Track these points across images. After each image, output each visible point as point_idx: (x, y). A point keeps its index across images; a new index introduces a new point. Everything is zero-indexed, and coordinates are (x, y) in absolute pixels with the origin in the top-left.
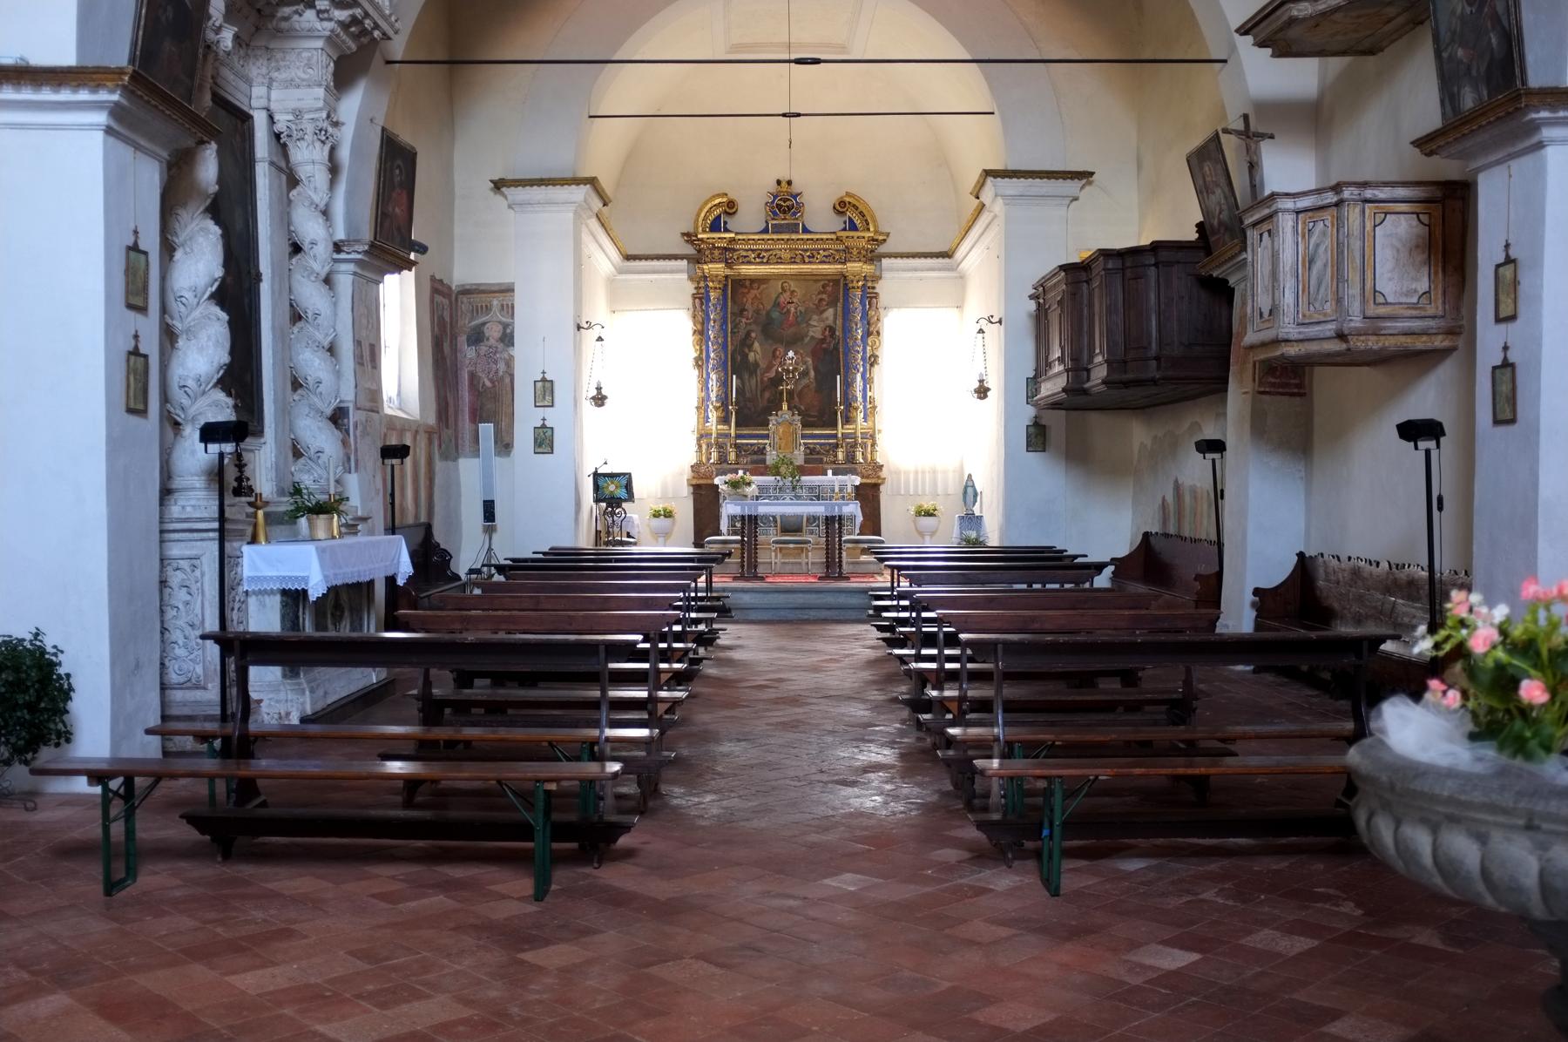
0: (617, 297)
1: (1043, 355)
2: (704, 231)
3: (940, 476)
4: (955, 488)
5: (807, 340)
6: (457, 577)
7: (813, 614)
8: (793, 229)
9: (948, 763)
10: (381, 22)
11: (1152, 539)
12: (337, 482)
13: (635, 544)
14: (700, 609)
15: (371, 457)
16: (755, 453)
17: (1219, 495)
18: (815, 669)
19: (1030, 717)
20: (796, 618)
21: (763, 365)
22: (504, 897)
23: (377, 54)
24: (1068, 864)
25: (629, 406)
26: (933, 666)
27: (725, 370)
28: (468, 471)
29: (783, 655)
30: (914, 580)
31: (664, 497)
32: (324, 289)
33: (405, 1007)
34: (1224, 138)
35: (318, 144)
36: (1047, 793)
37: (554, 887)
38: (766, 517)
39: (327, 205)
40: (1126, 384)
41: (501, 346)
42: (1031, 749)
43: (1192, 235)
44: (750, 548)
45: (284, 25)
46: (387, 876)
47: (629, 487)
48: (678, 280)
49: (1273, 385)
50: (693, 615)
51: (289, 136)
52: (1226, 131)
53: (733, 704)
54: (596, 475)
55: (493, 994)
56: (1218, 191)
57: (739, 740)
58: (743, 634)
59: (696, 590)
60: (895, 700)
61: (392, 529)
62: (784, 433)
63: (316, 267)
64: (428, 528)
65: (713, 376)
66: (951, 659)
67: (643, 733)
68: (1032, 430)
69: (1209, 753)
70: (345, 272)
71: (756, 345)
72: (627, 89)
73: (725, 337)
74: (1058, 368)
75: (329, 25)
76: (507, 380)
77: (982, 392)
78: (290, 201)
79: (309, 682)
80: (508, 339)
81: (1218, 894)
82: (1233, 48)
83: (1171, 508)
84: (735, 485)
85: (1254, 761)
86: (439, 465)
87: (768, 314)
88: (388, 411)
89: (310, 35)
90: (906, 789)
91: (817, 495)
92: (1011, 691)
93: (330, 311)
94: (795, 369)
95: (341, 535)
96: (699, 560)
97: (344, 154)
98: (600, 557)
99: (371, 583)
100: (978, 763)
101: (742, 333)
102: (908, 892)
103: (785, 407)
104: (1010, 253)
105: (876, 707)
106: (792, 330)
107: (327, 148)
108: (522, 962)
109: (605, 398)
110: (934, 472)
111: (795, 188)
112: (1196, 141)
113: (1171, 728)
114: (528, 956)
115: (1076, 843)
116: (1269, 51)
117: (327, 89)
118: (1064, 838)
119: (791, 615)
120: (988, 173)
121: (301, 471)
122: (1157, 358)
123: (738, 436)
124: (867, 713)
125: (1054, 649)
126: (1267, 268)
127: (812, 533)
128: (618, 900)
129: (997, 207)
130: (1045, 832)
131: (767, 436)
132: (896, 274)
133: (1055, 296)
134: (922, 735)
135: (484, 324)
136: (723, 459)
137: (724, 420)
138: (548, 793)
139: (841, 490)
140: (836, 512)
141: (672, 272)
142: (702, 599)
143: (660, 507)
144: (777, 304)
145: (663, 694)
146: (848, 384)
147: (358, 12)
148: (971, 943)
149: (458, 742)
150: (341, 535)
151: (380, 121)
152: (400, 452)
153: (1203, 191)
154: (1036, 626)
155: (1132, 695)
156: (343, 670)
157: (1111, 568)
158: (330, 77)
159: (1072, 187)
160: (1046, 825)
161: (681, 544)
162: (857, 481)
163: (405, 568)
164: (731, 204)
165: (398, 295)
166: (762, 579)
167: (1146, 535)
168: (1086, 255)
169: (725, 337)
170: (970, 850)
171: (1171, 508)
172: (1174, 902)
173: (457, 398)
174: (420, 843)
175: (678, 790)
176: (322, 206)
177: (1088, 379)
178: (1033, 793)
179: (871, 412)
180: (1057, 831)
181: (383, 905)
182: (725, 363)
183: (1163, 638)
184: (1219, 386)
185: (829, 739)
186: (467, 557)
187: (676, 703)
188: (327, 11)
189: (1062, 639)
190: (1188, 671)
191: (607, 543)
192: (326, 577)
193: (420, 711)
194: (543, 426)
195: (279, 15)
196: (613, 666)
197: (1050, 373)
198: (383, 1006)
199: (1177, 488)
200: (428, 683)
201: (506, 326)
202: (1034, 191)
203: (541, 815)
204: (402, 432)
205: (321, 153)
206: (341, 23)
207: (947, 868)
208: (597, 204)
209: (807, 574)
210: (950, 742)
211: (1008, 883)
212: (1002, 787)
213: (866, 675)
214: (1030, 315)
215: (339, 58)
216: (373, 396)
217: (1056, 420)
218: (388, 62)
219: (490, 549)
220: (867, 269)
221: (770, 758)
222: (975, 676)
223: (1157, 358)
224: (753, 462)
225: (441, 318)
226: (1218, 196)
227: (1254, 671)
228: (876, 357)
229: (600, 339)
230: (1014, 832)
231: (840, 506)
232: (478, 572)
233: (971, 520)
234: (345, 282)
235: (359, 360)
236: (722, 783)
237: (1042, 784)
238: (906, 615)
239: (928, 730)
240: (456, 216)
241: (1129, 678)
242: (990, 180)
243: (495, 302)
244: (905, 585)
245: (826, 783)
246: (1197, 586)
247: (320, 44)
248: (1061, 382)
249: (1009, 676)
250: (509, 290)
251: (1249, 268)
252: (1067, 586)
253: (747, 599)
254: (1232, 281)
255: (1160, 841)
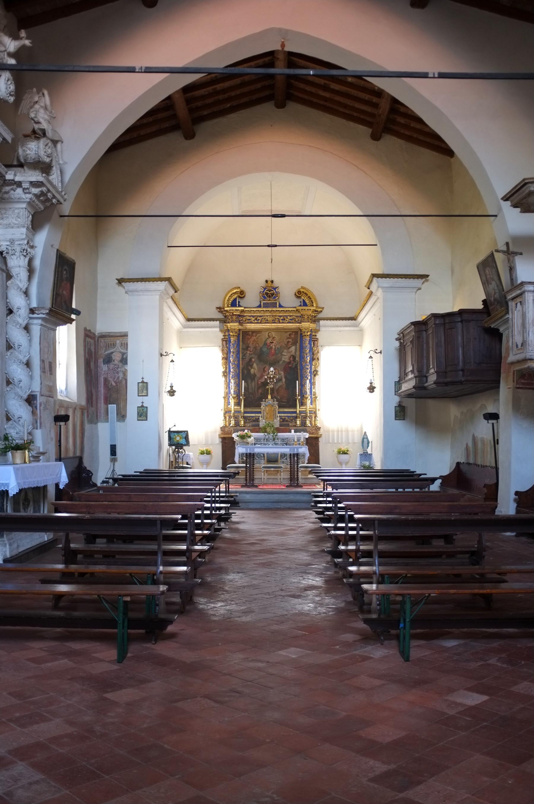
0: (183, 340)
1: (403, 370)
2: (228, 306)
3: (350, 433)
4: (358, 439)
5: (281, 362)
6: (95, 485)
7: (283, 505)
8: (274, 305)
9: (350, 585)
10: (56, 195)
11: (461, 466)
12: (30, 434)
13: (191, 468)
14: (222, 502)
15: (48, 419)
16: (254, 421)
17: (496, 442)
18: (282, 534)
19: (395, 560)
20: (274, 507)
21: (258, 375)
22: (100, 660)
23: (55, 212)
24: (414, 643)
25: (189, 395)
26: (343, 532)
27: (239, 378)
28: (103, 428)
29: (266, 527)
30: (334, 487)
31: (206, 444)
32: (24, 332)
33: (35, 727)
34: (496, 255)
35: (22, 257)
36: (403, 603)
37: (129, 655)
38: (259, 454)
39: (27, 289)
40: (447, 384)
41: (120, 364)
42: (394, 579)
43: (480, 306)
44: (250, 471)
45: (6, 196)
46: (37, 648)
47: (187, 438)
48: (214, 331)
49: (523, 384)
50: (218, 505)
51: (7, 253)
52: (497, 251)
53: (236, 553)
54: (170, 432)
55: (87, 718)
56: (494, 283)
57: (239, 573)
58: (246, 516)
59: (220, 492)
60: (323, 551)
61: (59, 459)
62: (269, 411)
63: (20, 321)
64: (81, 459)
65: (232, 381)
66: (352, 529)
67: (184, 568)
68: (398, 409)
69: (491, 581)
70: (36, 324)
71: (255, 365)
72: (189, 232)
73: (239, 361)
74: (410, 376)
75: (29, 196)
76: (124, 382)
77: (372, 389)
78: (7, 287)
79: (9, 540)
80: (124, 361)
81: (498, 661)
82: (500, 209)
83: (471, 449)
84: (242, 437)
85: (516, 586)
86: (87, 426)
87: (261, 349)
88: (60, 397)
89: (19, 201)
90: (328, 600)
91: (286, 442)
92: (382, 547)
93: (27, 345)
94: (274, 377)
95: (30, 462)
96: (221, 476)
97: (37, 263)
98: (171, 474)
99: (45, 487)
100: (365, 586)
101: (247, 359)
102: (326, 658)
103: (269, 397)
104: (386, 317)
105: (314, 555)
106: (274, 357)
107: (27, 259)
108: (106, 699)
109: (174, 391)
110: (347, 431)
111: (275, 284)
112: (482, 257)
113: (471, 567)
114: (109, 696)
115: (419, 631)
116: (519, 210)
117: (28, 228)
118: (412, 628)
119: (271, 506)
120: (374, 276)
121: (10, 427)
122: (463, 370)
123: (245, 412)
124: (308, 558)
125: (406, 523)
126: (520, 321)
127: (283, 462)
128: (163, 662)
129: (379, 293)
130: (402, 625)
131: (260, 412)
132: (327, 329)
133: (409, 338)
134: (337, 570)
135: (112, 353)
136: (237, 424)
137: (238, 404)
138: (125, 602)
139: (298, 440)
140: (296, 452)
141: (211, 327)
142: (223, 497)
143: (204, 449)
144: (265, 344)
145: (197, 547)
146: (302, 385)
147: (44, 189)
148: (359, 689)
149: (87, 573)
150: (30, 462)
151: (57, 246)
152: (65, 418)
153: (485, 283)
154: (397, 511)
155: (450, 548)
156: (28, 533)
157: (440, 481)
158: (29, 223)
159: (417, 283)
160: (402, 621)
161: (215, 468)
162: (307, 435)
163: (64, 479)
164: (242, 292)
165: (66, 337)
166: (256, 486)
167: (458, 464)
168: (424, 317)
169: (239, 361)
170: (361, 635)
171: (471, 449)
172: (473, 665)
173: (97, 391)
174: (59, 630)
175: (202, 600)
176: (24, 289)
177: (427, 381)
178: (395, 603)
179: (314, 400)
180: (408, 624)
181: (33, 665)
182: (239, 374)
183: (466, 517)
184: (493, 385)
185: (287, 572)
186: (101, 473)
187: (202, 553)
188: (28, 189)
189: (410, 517)
190: (480, 536)
191: (176, 468)
192: (18, 484)
193: (63, 556)
194: (142, 406)
195: (3, 191)
196: (165, 532)
197: (407, 378)
198: (22, 726)
199: (474, 439)
200: (68, 541)
201: (123, 354)
202: (398, 285)
203: (121, 615)
204: (67, 409)
205: (24, 262)
206: (35, 195)
207: (348, 645)
208: (171, 292)
209: (280, 484)
210: (351, 574)
211: (381, 654)
212: (378, 599)
213: (309, 537)
214: (396, 349)
215: (34, 213)
216: (51, 389)
217: (410, 404)
218: (61, 216)
219: (113, 470)
220: (312, 326)
221: (255, 582)
222: (365, 538)
223: (463, 370)
224: (253, 426)
225: (90, 350)
226: (493, 285)
227: (516, 536)
228: (317, 371)
229: (172, 361)
230: (385, 624)
231: (298, 448)
232: (107, 482)
233: (366, 456)
234: (36, 329)
235: (43, 370)
236: (227, 596)
237: (399, 598)
238: (330, 505)
239: (340, 567)
240: (99, 297)
241: (448, 539)
242: (375, 279)
243: (118, 342)
244: (330, 490)
245: (284, 596)
246: (485, 490)
247: (24, 205)
248: (412, 383)
249: (381, 538)
250: (125, 335)
251: (510, 321)
252: (416, 490)
253: (248, 497)
254: (501, 330)
255: (465, 630)
